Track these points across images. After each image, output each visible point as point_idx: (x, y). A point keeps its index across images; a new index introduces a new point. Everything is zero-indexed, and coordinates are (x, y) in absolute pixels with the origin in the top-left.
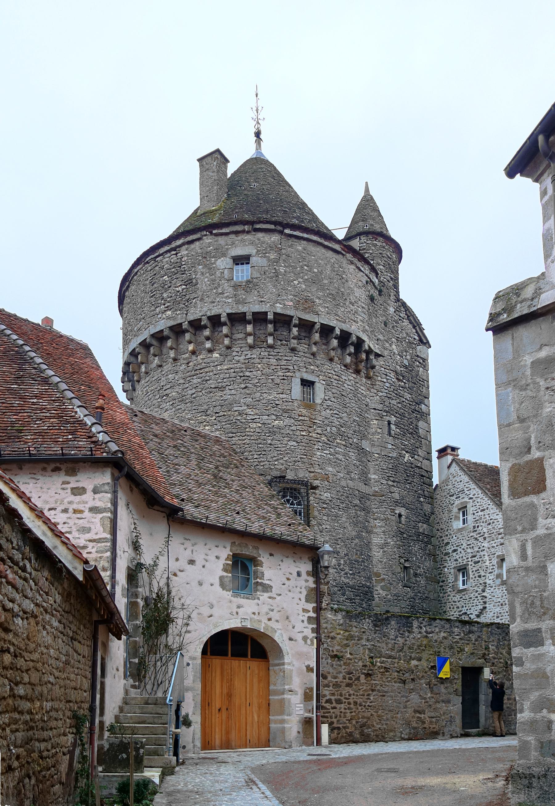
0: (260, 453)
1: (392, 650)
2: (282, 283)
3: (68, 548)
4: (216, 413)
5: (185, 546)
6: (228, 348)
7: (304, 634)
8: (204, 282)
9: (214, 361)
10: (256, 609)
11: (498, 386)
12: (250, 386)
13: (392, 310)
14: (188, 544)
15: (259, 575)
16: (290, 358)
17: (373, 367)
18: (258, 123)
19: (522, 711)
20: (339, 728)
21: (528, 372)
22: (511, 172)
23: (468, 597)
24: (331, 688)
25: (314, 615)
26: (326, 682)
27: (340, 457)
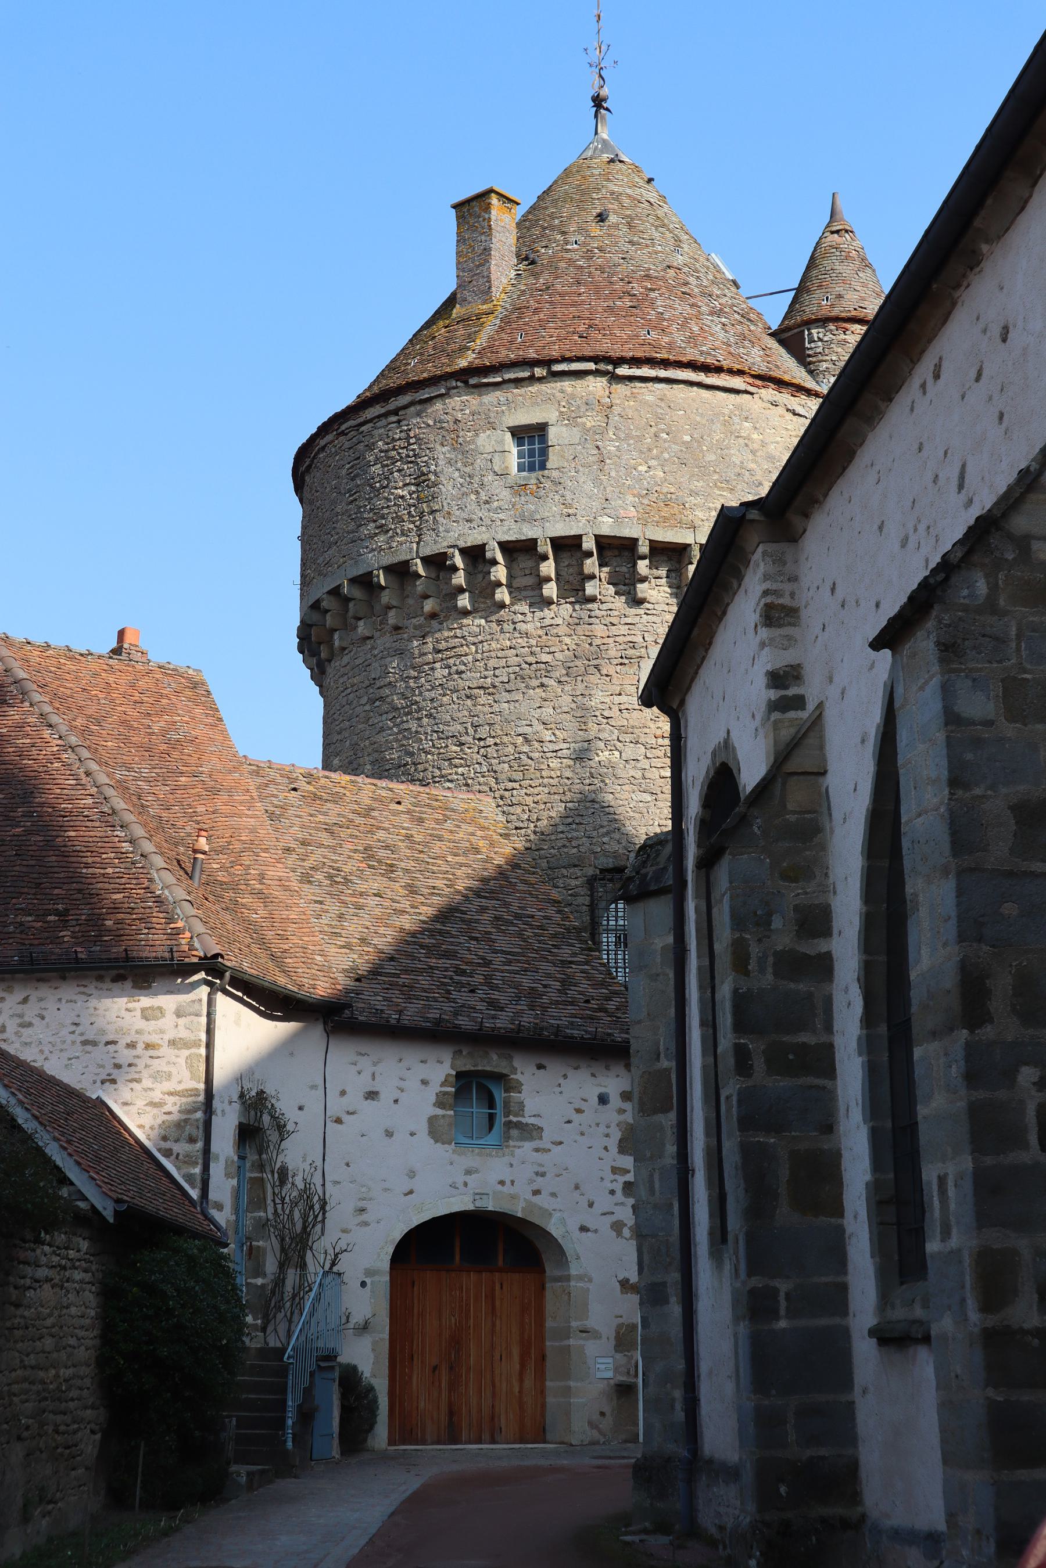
2: (613, 474)
3: (97, 1185)
4: (480, 739)
5: (358, 1067)
10: (507, 1176)
12: (551, 682)
14: (365, 1063)
15: (514, 1107)
21: (658, 959)
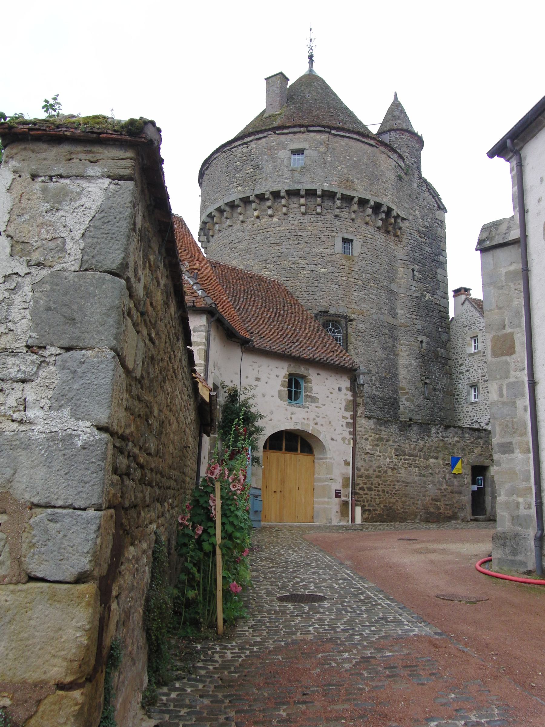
1: (414, 449)
6: (285, 214)
7: (342, 436)
8: (268, 167)
9: (273, 223)
11: (484, 285)
13: (415, 185)
14: (256, 366)
15: (309, 389)
17: (400, 228)
18: (311, 49)
19: (500, 496)
20: (369, 510)
21: (503, 278)
22: (492, 154)
23: (478, 409)
24: (364, 478)
25: (352, 421)
26: (360, 473)
27: (373, 297)
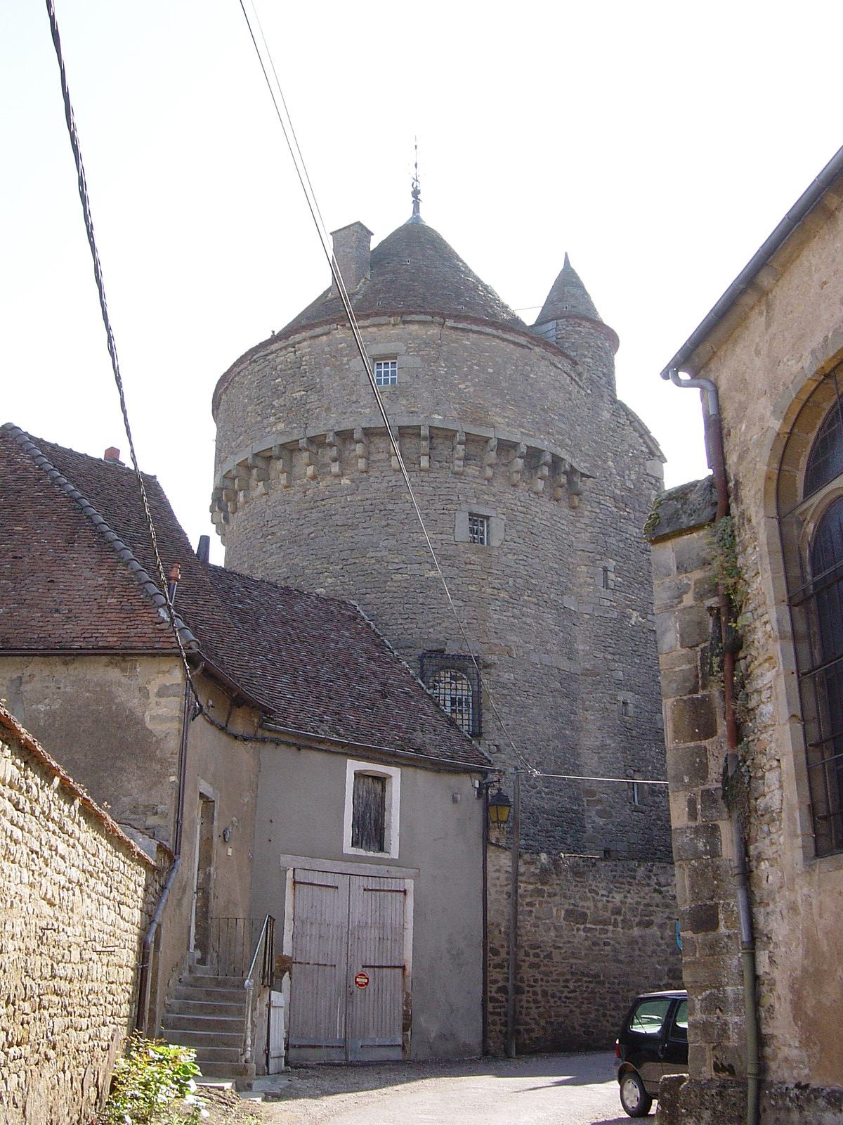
0: (407, 616)
13: (606, 415)
16: (453, 486)
26: (497, 960)
